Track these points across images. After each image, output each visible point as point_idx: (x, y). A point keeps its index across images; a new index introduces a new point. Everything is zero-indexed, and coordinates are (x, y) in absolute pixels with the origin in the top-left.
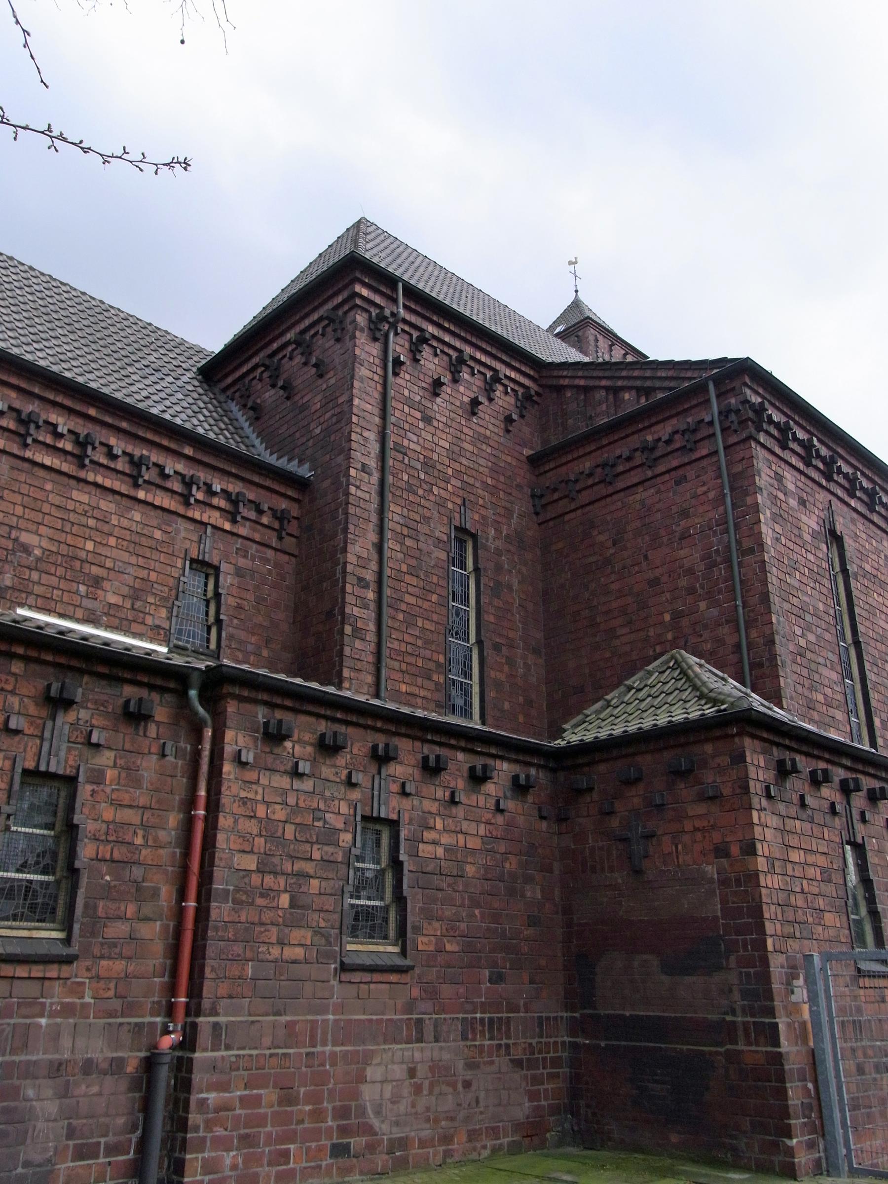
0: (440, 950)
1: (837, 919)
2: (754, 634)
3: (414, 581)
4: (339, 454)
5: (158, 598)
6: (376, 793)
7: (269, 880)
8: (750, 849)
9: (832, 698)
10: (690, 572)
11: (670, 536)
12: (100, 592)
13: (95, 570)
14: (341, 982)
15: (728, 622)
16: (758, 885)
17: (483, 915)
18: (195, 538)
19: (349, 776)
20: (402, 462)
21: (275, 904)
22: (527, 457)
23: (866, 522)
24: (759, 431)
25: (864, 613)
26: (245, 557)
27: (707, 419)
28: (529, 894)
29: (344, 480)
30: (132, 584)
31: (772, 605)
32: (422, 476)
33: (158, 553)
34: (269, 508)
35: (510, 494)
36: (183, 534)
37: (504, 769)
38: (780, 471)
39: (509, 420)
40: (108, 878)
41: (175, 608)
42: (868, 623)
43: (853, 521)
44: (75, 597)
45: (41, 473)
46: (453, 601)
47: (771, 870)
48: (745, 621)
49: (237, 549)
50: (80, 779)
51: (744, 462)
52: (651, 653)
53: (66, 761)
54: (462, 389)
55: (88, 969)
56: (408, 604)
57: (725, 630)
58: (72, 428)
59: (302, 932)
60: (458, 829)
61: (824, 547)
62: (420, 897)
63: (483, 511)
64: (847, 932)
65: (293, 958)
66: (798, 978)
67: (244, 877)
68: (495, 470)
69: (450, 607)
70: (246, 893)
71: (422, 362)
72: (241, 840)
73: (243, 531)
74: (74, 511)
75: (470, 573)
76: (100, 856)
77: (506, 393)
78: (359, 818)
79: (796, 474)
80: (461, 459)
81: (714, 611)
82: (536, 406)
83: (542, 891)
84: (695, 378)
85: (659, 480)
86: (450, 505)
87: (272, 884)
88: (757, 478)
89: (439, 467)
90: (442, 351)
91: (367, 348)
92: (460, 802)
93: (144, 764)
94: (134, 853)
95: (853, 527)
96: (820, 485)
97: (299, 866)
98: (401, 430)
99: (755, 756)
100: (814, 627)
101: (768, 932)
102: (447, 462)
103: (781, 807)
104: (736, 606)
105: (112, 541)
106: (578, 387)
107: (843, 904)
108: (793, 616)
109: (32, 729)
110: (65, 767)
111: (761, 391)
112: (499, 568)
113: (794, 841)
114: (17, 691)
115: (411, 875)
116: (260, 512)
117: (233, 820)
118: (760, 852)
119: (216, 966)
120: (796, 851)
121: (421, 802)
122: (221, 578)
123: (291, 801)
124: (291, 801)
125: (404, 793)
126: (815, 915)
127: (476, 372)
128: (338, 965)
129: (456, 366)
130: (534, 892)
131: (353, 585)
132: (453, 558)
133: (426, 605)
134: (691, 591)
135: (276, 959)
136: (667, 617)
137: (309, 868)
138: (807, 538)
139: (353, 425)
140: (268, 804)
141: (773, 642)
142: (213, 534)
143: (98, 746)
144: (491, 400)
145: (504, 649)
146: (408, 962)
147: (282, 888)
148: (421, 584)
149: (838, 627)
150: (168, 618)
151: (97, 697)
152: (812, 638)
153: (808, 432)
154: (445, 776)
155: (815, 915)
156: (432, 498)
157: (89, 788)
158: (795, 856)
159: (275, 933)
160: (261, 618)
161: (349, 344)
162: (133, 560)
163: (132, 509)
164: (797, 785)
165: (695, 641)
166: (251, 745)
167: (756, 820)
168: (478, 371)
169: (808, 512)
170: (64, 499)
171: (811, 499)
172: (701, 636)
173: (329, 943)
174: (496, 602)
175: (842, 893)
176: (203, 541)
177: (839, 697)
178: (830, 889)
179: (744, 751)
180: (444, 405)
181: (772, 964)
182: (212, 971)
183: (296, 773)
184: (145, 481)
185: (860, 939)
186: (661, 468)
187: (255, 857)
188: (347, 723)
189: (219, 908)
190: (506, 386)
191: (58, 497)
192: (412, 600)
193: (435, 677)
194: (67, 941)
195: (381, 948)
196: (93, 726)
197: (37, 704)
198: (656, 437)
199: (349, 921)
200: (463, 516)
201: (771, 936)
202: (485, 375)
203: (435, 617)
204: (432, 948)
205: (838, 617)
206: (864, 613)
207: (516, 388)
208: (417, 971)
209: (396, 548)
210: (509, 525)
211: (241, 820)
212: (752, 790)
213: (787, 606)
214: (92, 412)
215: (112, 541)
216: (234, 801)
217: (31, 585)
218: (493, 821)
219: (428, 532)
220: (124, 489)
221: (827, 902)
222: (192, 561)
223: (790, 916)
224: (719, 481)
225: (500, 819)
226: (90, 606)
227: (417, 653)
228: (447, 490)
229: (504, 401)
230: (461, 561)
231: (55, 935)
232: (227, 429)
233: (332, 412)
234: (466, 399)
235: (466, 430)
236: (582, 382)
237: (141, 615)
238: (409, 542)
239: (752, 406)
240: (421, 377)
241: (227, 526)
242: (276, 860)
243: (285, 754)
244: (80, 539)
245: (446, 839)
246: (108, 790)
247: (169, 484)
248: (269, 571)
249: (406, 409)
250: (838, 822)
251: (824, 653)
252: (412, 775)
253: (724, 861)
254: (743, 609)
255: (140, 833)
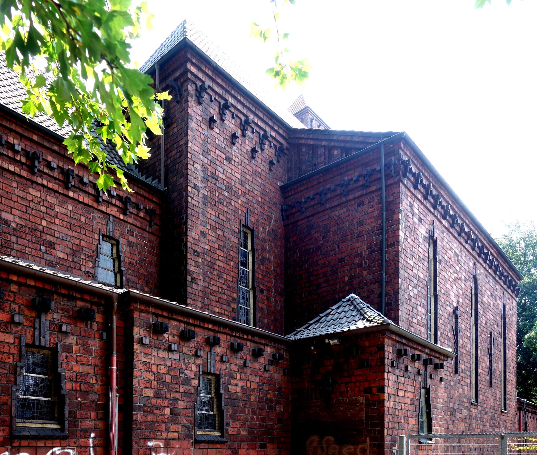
0: (238, 434)
1: (414, 421)
2: (389, 288)
3: (221, 253)
4: (181, 178)
5: (86, 256)
6: (209, 361)
7: (160, 401)
8: (382, 390)
9: (421, 322)
10: (361, 255)
11: (352, 235)
12: (53, 251)
13: (49, 238)
14: (195, 448)
15: (377, 282)
16: (383, 406)
17: (257, 418)
18: (104, 223)
19: (196, 352)
20: (215, 184)
21: (163, 413)
22: (280, 187)
23: (449, 233)
24: (404, 178)
25: (441, 281)
26: (132, 235)
27: (378, 168)
28: (278, 409)
29: (184, 193)
30: (71, 247)
31: (400, 274)
32: (226, 194)
33: (84, 230)
34: (144, 208)
35: (271, 208)
36: (97, 220)
37: (268, 350)
38: (412, 202)
39: (271, 163)
40: (79, 399)
41: (97, 262)
42: (442, 286)
43: (443, 232)
44: (39, 253)
45: (8, 176)
46: (241, 266)
47: (390, 399)
48: (386, 282)
49: (128, 230)
50: (59, 350)
51: (395, 195)
52: (337, 297)
53: (50, 341)
54: (247, 142)
55: (75, 443)
56: (219, 266)
57: (375, 286)
58: (24, 148)
59: (177, 426)
60: (247, 379)
61: (427, 245)
62: (229, 410)
63: (257, 217)
64: (417, 426)
65: (173, 437)
66: (395, 446)
67: (148, 400)
68: (263, 193)
69: (240, 269)
70: (149, 407)
71: (225, 122)
72: (145, 382)
73: (131, 220)
74: (32, 201)
75: (249, 251)
76: (74, 388)
77: (271, 146)
78: (201, 373)
79: (419, 204)
80: (246, 186)
81: (370, 276)
82: (286, 156)
83: (284, 407)
84: (373, 143)
85: (349, 203)
86: (240, 212)
87: (162, 403)
88: (400, 205)
89: (235, 189)
90: (237, 116)
91: (195, 109)
92: (248, 366)
93: (92, 343)
94: (92, 388)
95: (442, 236)
96: (430, 211)
97: (174, 395)
98: (215, 165)
99: (389, 347)
100: (417, 286)
101: (386, 427)
102: (239, 186)
103: (397, 371)
104: (382, 274)
105: (57, 221)
106: (309, 145)
107: (417, 414)
108: (409, 280)
109: (28, 322)
110: (50, 343)
111: (408, 153)
112: (264, 249)
113: (400, 386)
114: (16, 302)
115: (226, 400)
116: (139, 210)
117: (140, 372)
118: (386, 391)
119: (137, 441)
120: (401, 391)
121: (230, 366)
122: (120, 247)
123: (169, 364)
124: (169, 364)
125: (222, 361)
126: (405, 419)
127: (255, 131)
128: (193, 441)
129: (244, 125)
130: (280, 408)
131: (191, 254)
132: (241, 242)
133: (228, 267)
134: (360, 265)
135: (165, 438)
136: (347, 278)
137: (178, 396)
138: (420, 240)
139: (189, 159)
140: (157, 365)
141: (398, 293)
142: (114, 221)
143: (66, 333)
144: (262, 150)
145: (265, 292)
146: (224, 440)
147: (166, 405)
148: (226, 255)
149: (428, 287)
150: (93, 268)
151: (62, 307)
152: (416, 291)
153: (428, 180)
154: (241, 353)
155: (405, 419)
156: (231, 207)
157: (64, 354)
158: (401, 393)
159: (164, 426)
160: (143, 270)
161: (184, 105)
162: (70, 233)
163: (66, 202)
164: (405, 360)
165: (360, 291)
166: (147, 335)
167: (386, 377)
168: (256, 131)
169: (422, 225)
170: (25, 194)
171: (424, 219)
172: (363, 289)
173: (189, 431)
174: (262, 267)
175: (417, 410)
176: (109, 225)
177: (425, 321)
178: (413, 408)
179: (384, 345)
180: (237, 151)
181: (385, 440)
182: (136, 444)
183: (169, 350)
184: (72, 186)
185: (422, 428)
186: (351, 197)
187: (153, 390)
188: (195, 326)
189: (137, 414)
190: (270, 142)
191: (21, 192)
192: (221, 264)
193: (232, 305)
194: (62, 430)
195: (212, 433)
196: (62, 322)
197: (29, 309)
198: (350, 178)
199: (198, 420)
200: (247, 219)
201: (386, 428)
202: (259, 134)
203: (232, 274)
204: (235, 433)
205: (428, 282)
206: (441, 281)
207: (276, 144)
208: (229, 443)
209: (212, 235)
210: (270, 225)
211: (145, 373)
212: (386, 363)
213: (407, 275)
214: (35, 138)
215: (57, 221)
216: (141, 363)
217: (12, 244)
218: (263, 376)
219: (229, 227)
220: (60, 190)
221: (411, 413)
222: (104, 236)
223: (395, 419)
224: (380, 205)
225: (266, 375)
226: (48, 258)
227: (224, 292)
228: (238, 203)
229: (269, 151)
230: (245, 244)
231: (55, 426)
232: (115, 158)
233: (176, 150)
234: (249, 148)
235: (249, 168)
236: (312, 142)
237: (78, 265)
238: (219, 232)
239: (403, 162)
240: (225, 132)
241: (121, 217)
242: (163, 392)
243: (165, 340)
244: (38, 218)
245: (241, 384)
246: (75, 356)
247: (87, 189)
248: (146, 245)
249: (217, 152)
250: (420, 379)
251: (421, 300)
252: (226, 352)
253: (369, 395)
254: (385, 275)
255: (94, 378)
